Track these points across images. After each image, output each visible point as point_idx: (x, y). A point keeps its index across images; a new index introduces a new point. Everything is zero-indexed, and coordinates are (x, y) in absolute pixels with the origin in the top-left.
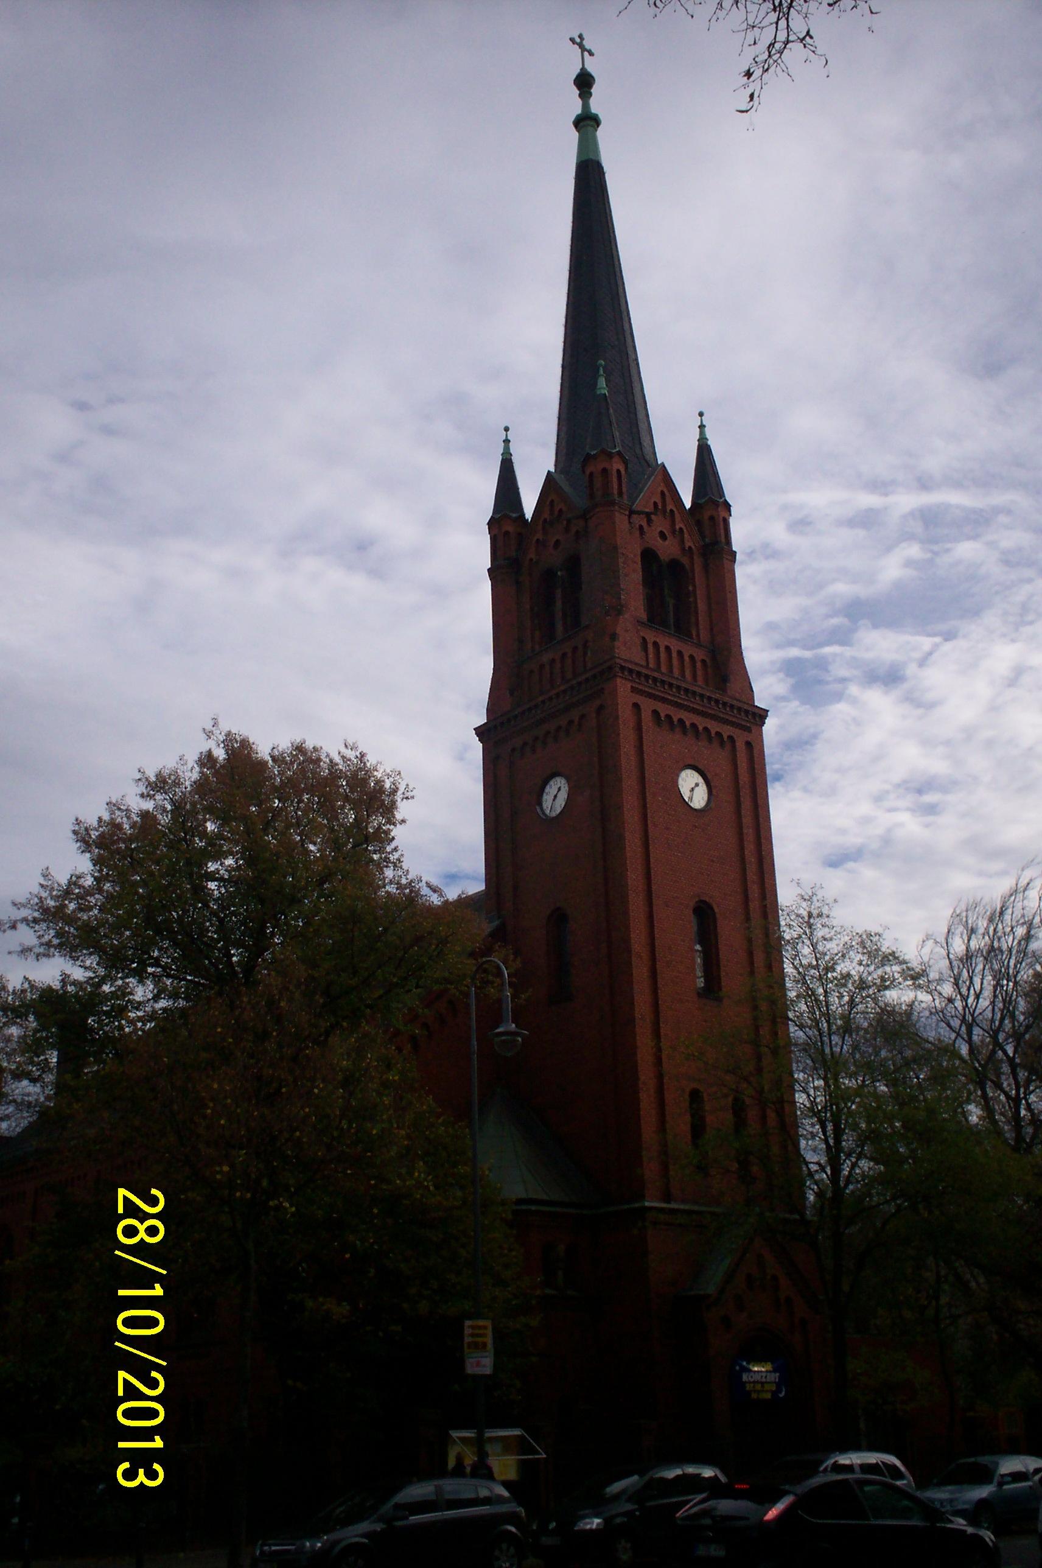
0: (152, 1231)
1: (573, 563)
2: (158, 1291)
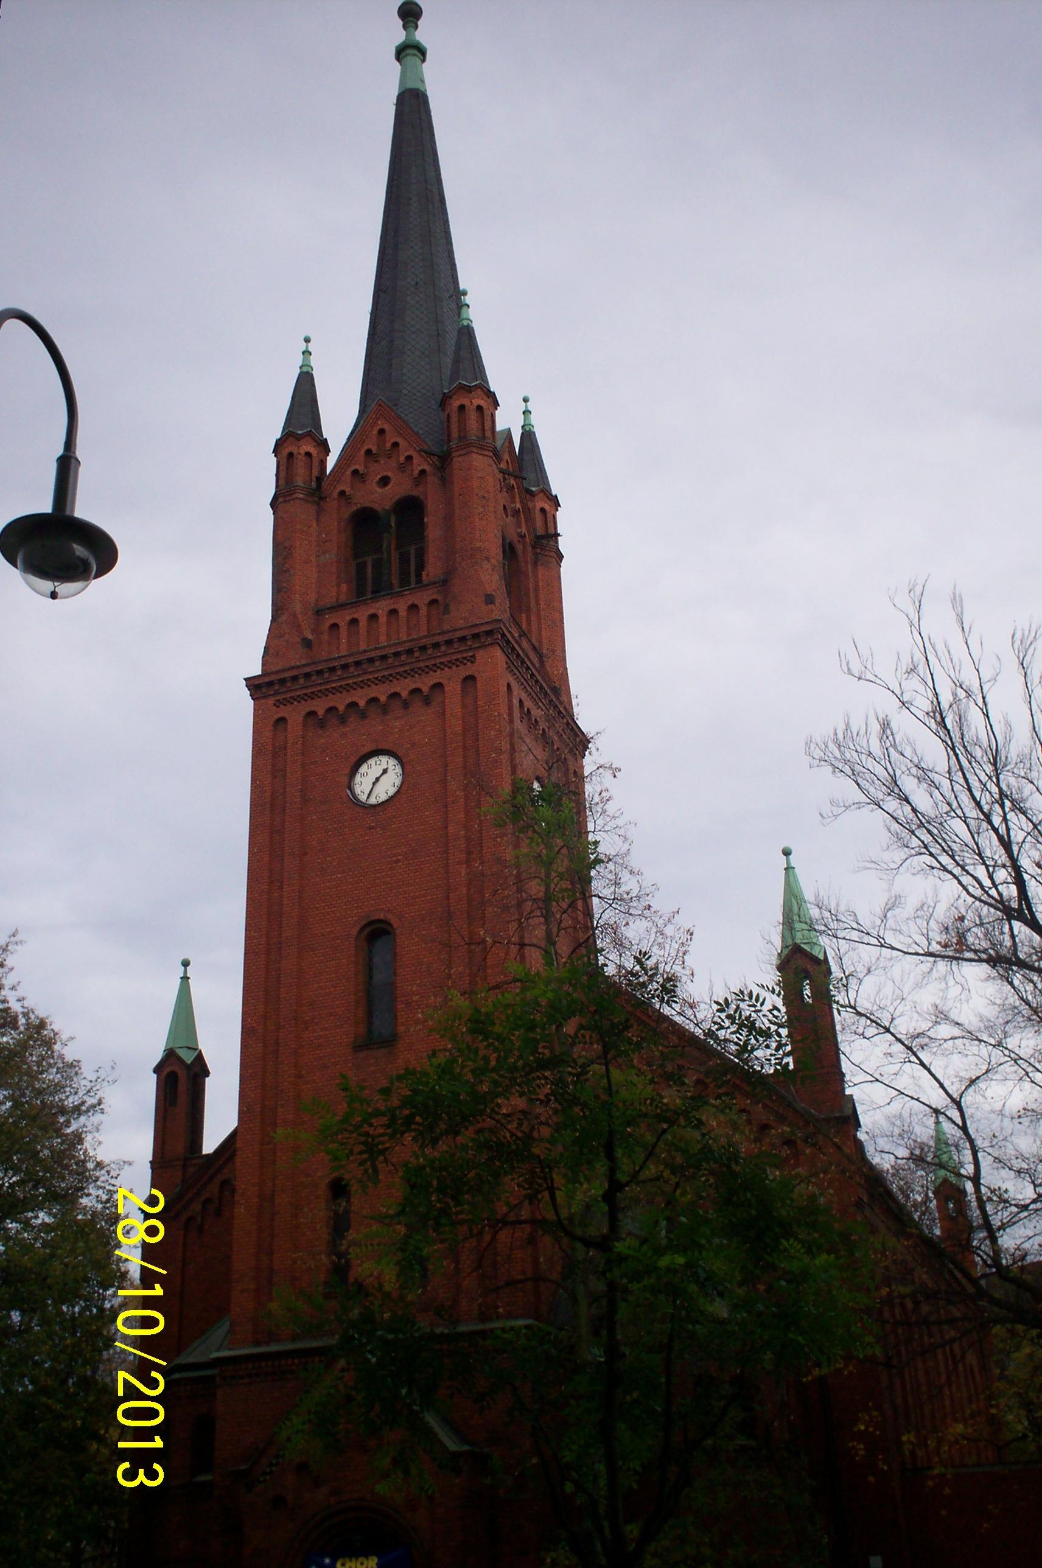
2: (158, 1291)
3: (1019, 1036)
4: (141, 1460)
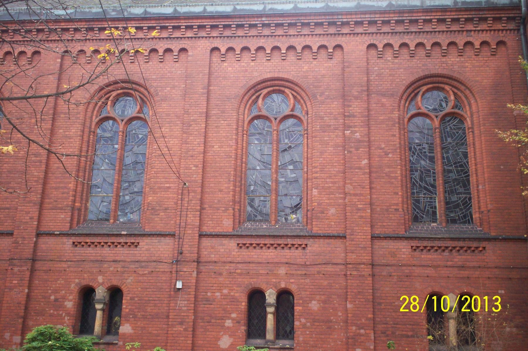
3: (60, 48)
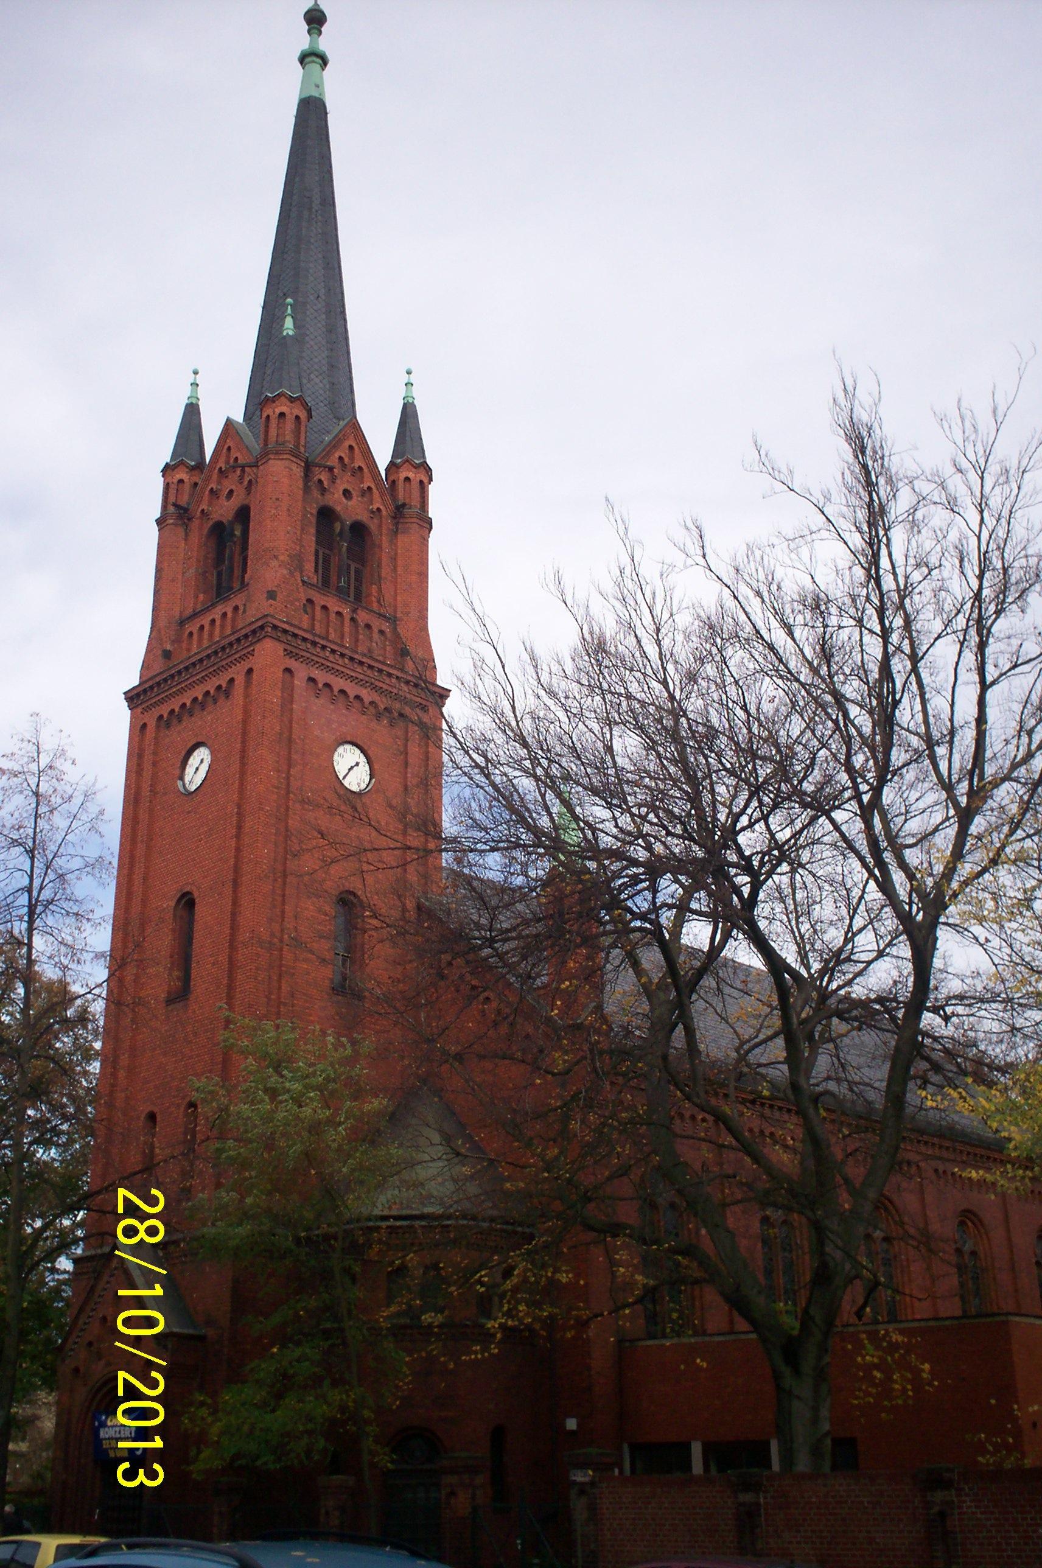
0: (152, 1231)
1: (243, 514)
2: (158, 1291)
4: (139, 1461)
